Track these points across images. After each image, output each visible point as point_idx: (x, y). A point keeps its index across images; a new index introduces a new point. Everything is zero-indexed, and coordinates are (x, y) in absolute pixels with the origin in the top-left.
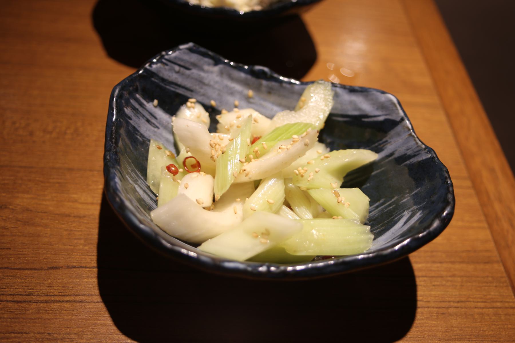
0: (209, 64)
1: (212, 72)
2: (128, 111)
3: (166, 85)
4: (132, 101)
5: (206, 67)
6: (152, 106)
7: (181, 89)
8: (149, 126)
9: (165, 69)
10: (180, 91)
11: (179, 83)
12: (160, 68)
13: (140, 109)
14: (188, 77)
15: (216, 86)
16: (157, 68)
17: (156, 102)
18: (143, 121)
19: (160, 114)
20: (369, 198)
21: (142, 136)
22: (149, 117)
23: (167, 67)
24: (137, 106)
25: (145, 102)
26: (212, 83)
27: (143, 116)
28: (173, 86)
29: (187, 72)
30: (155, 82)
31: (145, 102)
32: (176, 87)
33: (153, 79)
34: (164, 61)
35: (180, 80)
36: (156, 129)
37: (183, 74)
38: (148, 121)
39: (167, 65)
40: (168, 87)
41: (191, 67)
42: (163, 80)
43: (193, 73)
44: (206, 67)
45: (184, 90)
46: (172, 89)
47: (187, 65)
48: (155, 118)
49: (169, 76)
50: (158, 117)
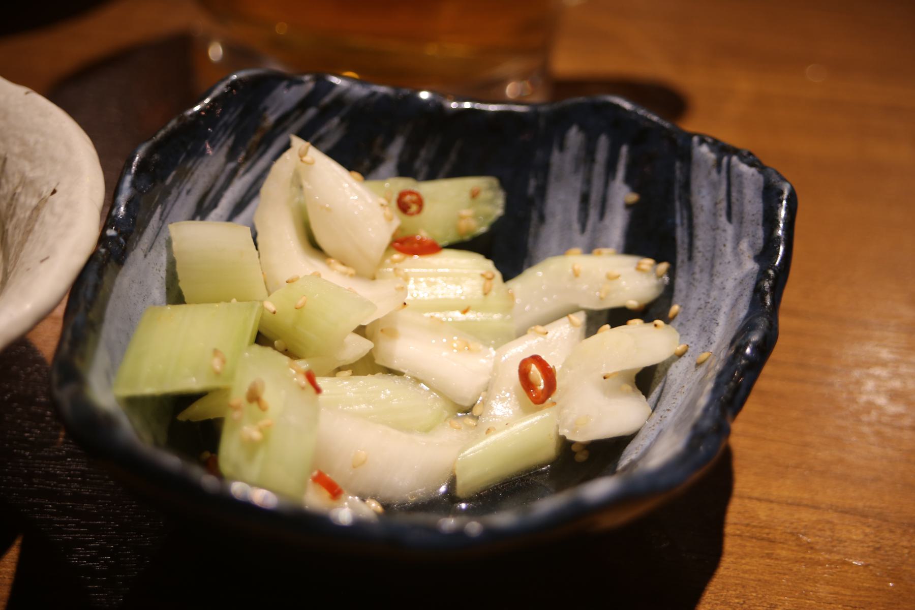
0: (752, 246)
1: (740, 264)
2: (574, 137)
3: (680, 198)
4: (603, 143)
5: (744, 245)
6: (622, 194)
7: (686, 234)
8: (575, 206)
9: (709, 173)
10: (681, 234)
11: (696, 221)
12: (706, 162)
13: (599, 168)
14: (715, 228)
15: (714, 293)
16: (783, 230)
17: (633, 198)
18: (576, 184)
19: (617, 223)
20: (294, 532)
21: (542, 191)
22: (595, 197)
23: (714, 174)
24: (601, 155)
25: (621, 173)
26: (717, 281)
27: (588, 181)
28: (685, 213)
29: (723, 219)
30: (673, 172)
31: (621, 173)
32: (685, 221)
33: (678, 164)
34: (725, 160)
35: (702, 219)
36: (576, 226)
37: (715, 215)
38: (585, 199)
39: (719, 171)
40: (678, 205)
41: (734, 219)
42: (687, 186)
43: (724, 231)
44: (744, 245)
45: (686, 240)
46: (678, 220)
47: (735, 209)
48: (602, 215)
49: (699, 192)
50: (607, 221)
